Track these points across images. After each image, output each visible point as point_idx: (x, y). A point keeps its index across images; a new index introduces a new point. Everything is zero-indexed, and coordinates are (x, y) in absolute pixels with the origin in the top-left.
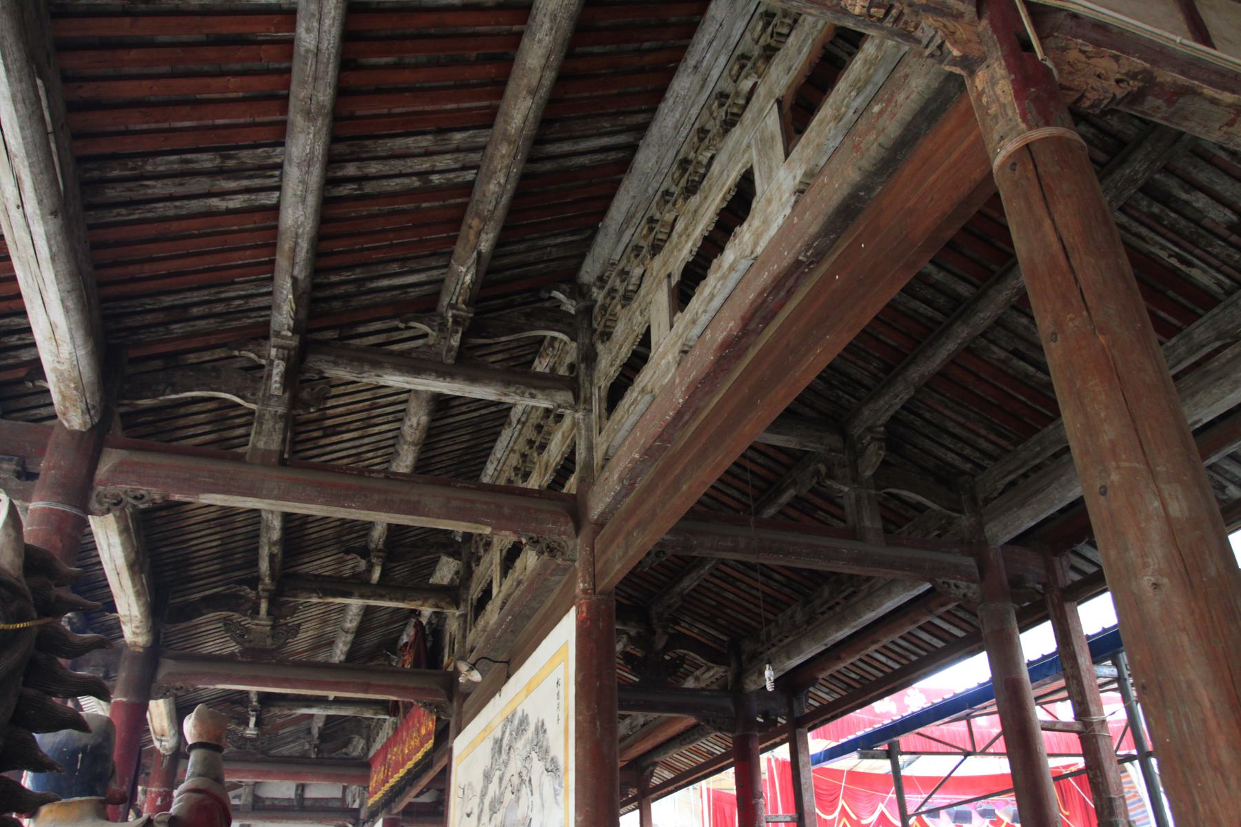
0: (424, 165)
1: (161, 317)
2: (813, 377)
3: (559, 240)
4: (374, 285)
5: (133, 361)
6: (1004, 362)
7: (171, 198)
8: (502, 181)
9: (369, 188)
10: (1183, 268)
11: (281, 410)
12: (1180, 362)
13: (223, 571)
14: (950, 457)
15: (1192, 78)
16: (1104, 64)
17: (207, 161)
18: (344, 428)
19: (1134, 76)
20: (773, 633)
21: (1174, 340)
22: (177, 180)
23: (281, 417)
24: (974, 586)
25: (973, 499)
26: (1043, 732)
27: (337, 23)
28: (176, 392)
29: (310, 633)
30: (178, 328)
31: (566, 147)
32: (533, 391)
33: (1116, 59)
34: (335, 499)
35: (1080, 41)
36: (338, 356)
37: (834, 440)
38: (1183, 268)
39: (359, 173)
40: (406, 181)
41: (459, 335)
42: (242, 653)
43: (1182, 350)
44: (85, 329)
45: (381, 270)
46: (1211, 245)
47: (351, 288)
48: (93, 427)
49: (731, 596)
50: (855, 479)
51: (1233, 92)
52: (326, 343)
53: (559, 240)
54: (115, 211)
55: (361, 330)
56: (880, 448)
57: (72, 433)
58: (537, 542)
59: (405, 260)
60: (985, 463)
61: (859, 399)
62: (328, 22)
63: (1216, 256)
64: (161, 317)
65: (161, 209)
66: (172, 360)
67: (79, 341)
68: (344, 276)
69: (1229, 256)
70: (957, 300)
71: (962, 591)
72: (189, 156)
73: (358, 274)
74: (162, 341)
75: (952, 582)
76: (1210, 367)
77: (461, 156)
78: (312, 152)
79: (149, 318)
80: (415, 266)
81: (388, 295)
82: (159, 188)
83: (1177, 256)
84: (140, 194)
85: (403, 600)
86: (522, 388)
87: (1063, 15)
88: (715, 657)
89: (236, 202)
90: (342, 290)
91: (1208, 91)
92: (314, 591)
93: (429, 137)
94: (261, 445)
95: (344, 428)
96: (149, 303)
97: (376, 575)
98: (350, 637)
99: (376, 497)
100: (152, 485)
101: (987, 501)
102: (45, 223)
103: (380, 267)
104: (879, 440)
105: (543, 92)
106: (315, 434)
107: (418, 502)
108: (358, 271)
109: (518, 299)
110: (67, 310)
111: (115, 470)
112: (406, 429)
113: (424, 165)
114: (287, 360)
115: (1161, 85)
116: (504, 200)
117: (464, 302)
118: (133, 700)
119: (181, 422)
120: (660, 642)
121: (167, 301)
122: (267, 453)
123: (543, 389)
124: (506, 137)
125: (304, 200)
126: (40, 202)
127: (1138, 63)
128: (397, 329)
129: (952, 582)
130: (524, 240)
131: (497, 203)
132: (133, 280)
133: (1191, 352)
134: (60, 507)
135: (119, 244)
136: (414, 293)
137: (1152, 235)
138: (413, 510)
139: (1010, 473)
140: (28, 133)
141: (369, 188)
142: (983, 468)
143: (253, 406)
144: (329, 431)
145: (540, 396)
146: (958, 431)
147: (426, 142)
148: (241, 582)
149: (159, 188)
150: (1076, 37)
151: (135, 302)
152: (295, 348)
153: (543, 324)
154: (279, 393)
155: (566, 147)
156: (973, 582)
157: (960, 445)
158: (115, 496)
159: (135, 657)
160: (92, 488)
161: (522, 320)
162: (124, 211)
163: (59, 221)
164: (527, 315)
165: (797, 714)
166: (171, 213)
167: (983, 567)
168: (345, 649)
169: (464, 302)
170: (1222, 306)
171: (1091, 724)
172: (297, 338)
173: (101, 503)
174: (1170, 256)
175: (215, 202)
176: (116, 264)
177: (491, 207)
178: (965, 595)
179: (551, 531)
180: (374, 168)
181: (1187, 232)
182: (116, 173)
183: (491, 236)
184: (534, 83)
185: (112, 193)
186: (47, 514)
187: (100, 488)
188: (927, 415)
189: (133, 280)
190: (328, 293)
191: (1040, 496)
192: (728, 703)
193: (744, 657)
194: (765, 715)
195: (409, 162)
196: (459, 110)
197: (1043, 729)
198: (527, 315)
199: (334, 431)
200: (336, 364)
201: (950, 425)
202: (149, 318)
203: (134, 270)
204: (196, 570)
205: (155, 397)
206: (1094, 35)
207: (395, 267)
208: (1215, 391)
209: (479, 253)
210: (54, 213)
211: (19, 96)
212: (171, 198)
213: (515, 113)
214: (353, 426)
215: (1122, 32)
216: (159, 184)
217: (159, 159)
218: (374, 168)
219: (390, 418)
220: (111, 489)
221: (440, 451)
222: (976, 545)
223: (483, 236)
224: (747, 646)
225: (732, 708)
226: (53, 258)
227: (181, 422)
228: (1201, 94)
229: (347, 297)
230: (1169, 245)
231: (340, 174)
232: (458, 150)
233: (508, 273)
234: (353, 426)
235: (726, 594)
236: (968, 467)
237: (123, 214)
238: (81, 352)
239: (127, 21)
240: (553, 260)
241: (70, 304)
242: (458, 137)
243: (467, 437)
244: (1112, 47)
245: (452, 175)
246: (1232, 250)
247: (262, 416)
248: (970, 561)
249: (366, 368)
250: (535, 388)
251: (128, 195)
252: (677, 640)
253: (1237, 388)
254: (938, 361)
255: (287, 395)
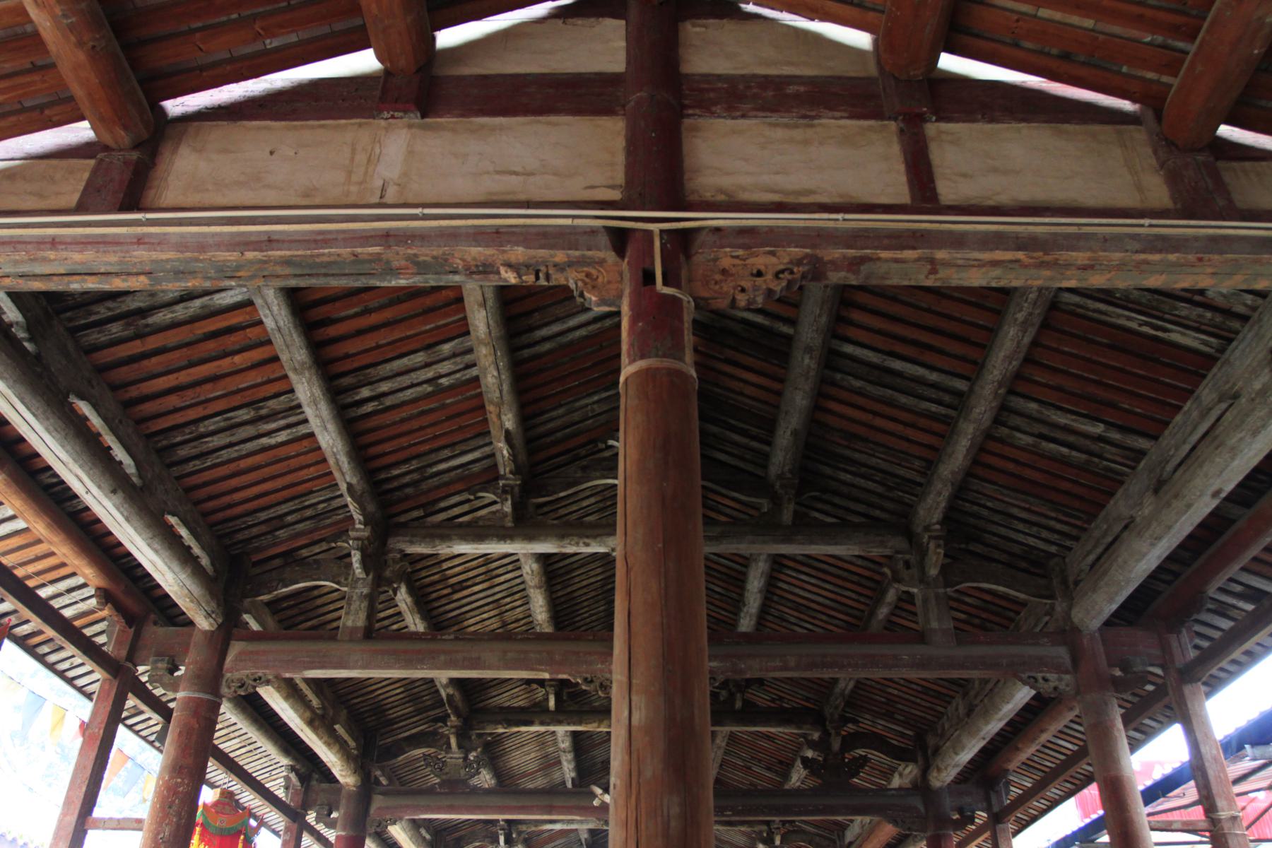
0: (430, 373)
1: (263, 528)
2: (1210, 376)
3: (596, 398)
4: (435, 469)
5: (255, 564)
6: (1033, 446)
7: (231, 445)
8: (495, 374)
9: (388, 401)
10: (1159, 334)
11: (366, 591)
12: (1195, 428)
13: (419, 712)
14: (1031, 541)
15: (862, 249)
16: (761, 261)
17: (244, 415)
18: (469, 583)
19: (799, 262)
20: (946, 726)
21: (1189, 404)
22: (228, 433)
23: (366, 596)
24: (1067, 677)
25: (1064, 582)
26: (1152, 833)
27: (283, 307)
28: (286, 586)
29: (533, 755)
30: (281, 533)
31: (556, 328)
32: (587, 540)
33: (773, 254)
34: (409, 664)
35: (728, 249)
36: (413, 536)
37: (898, 542)
38: (1159, 334)
39: (373, 394)
40: (419, 389)
41: (509, 502)
42: (441, 785)
43: (1195, 414)
44: (179, 559)
45: (434, 457)
46: (1176, 309)
47: (416, 476)
48: (220, 626)
49: (896, 692)
50: (923, 579)
51: (914, 248)
52: (404, 525)
53: (596, 398)
54: (191, 464)
55: (443, 504)
56: (938, 546)
57: (205, 633)
58: (592, 681)
59: (453, 445)
60: (1068, 543)
61: (916, 496)
62: (275, 308)
63: (1186, 318)
64: (263, 528)
65: (225, 455)
66: (290, 557)
67: (177, 568)
68: (404, 469)
69: (1200, 316)
70: (959, 394)
71: (1052, 684)
72: (229, 415)
73: (415, 464)
74: (275, 545)
75: (1039, 676)
76: (1217, 432)
77: (458, 359)
78: (312, 394)
79: (255, 531)
80: (464, 448)
81: (453, 474)
82: (216, 441)
83: (1147, 324)
84: (204, 448)
85: (580, 723)
86: (576, 539)
87: (704, 233)
88: (903, 755)
89: (282, 437)
90: (407, 479)
91: (884, 254)
92: (499, 723)
93: (421, 354)
94: (349, 623)
95: (469, 583)
96: (250, 520)
97: (552, 703)
98: (570, 756)
99: (442, 658)
100: (266, 667)
101: (1077, 583)
102: (110, 499)
103: (433, 455)
104: (936, 538)
105: (490, 303)
106: (445, 592)
107: (479, 658)
108: (414, 462)
109: (583, 452)
110: (156, 551)
111: (238, 658)
112: (527, 578)
113: (430, 373)
114: (363, 550)
115: (832, 262)
116: (505, 387)
117: (511, 472)
118: (351, 833)
119: (319, 602)
120: (836, 745)
121: (263, 516)
122: (354, 630)
123: (595, 537)
124: (481, 342)
125: (326, 428)
126: (99, 487)
127: (796, 251)
128: (468, 501)
129: (1039, 676)
130: (561, 406)
131: (501, 392)
132: (230, 506)
133: (1203, 415)
134: (196, 695)
135: (205, 484)
136: (476, 468)
137: (1111, 309)
138: (475, 665)
139: (1089, 553)
140: (69, 448)
141: (388, 401)
142: (1070, 549)
143: (345, 589)
144: (457, 587)
145: (593, 544)
146: (1024, 515)
147: (420, 358)
148: (436, 720)
149: (216, 441)
150: (723, 247)
151: (238, 522)
152: (368, 538)
153: (598, 474)
154: (363, 576)
155: (556, 328)
156: (1067, 672)
157: (1035, 529)
158: (240, 680)
159: (350, 794)
160: (222, 676)
161: (579, 474)
162: (197, 462)
163: (120, 494)
164: (584, 468)
165: (996, 809)
166: (235, 455)
167: (1076, 658)
168: (572, 766)
169: (511, 472)
170: (1219, 364)
171: (1220, 821)
172: (369, 528)
173: (229, 687)
174: (1140, 325)
175: (265, 441)
176: (211, 498)
177: (497, 394)
178: (1055, 688)
179: (602, 671)
180: (385, 387)
181: (1144, 301)
182: (179, 439)
183: (510, 416)
184: (480, 298)
185: (183, 452)
186: (188, 700)
187: (229, 675)
188: (989, 504)
189: (230, 506)
190: (395, 484)
191: (1106, 579)
192: (918, 803)
193: (929, 752)
194: (960, 811)
195: (413, 375)
196: (438, 328)
197: (1152, 829)
198: (584, 468)
199: (461, 586)
200: (412, 542)
201: (1015, 511)
202: (255, 531)
203: (226, 500)
204: (393, 714)
205: (270, 592)
206: (741, 241)
207: (447, 453)
208: (1218, 460)
209: (507, 432)
210: (114, 492)
211: (51, 428)
212: (231, 445)
213: (477, 322)
214: (478, 579)
215: (771, 230)
216: (215, 438)
217: (206, 423)
218: (385, 387)
219: (510, 568)
220: (237, 675)
221: (579, 585)
222: (1069, 635)
223: (503, 417)
224: (931, 741)
225: (922, 809)
226: (127, 519)
227: (319, 602)
228: (879, 259)
229: (414, 483)
230: (1133, 315)
231: (357, 398)
232: (454, 355)
233: (559, 435)
234: (478, 579)
235: (890, 690)
236: (1053, 549)
237: (196, 465)
238: (183, 576)
239: (138, 342)
240: (599, 414)
241: (156, 546)
242: (447, 348)
243: (599, 570)
244: (762, 245)
245: (458, 375)
246: (1200, 310)
247: (350, 598)
248: (1062, 653)
249: (437, 542)
250: (587, 537)
251: (194, 452)
252: (851, 741)
253: (1235, 455)
254: (961, 457)
255: (371, 577)
